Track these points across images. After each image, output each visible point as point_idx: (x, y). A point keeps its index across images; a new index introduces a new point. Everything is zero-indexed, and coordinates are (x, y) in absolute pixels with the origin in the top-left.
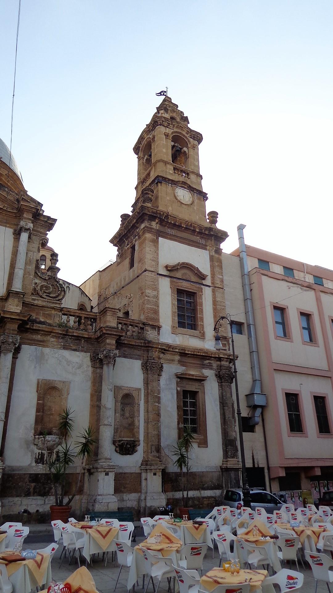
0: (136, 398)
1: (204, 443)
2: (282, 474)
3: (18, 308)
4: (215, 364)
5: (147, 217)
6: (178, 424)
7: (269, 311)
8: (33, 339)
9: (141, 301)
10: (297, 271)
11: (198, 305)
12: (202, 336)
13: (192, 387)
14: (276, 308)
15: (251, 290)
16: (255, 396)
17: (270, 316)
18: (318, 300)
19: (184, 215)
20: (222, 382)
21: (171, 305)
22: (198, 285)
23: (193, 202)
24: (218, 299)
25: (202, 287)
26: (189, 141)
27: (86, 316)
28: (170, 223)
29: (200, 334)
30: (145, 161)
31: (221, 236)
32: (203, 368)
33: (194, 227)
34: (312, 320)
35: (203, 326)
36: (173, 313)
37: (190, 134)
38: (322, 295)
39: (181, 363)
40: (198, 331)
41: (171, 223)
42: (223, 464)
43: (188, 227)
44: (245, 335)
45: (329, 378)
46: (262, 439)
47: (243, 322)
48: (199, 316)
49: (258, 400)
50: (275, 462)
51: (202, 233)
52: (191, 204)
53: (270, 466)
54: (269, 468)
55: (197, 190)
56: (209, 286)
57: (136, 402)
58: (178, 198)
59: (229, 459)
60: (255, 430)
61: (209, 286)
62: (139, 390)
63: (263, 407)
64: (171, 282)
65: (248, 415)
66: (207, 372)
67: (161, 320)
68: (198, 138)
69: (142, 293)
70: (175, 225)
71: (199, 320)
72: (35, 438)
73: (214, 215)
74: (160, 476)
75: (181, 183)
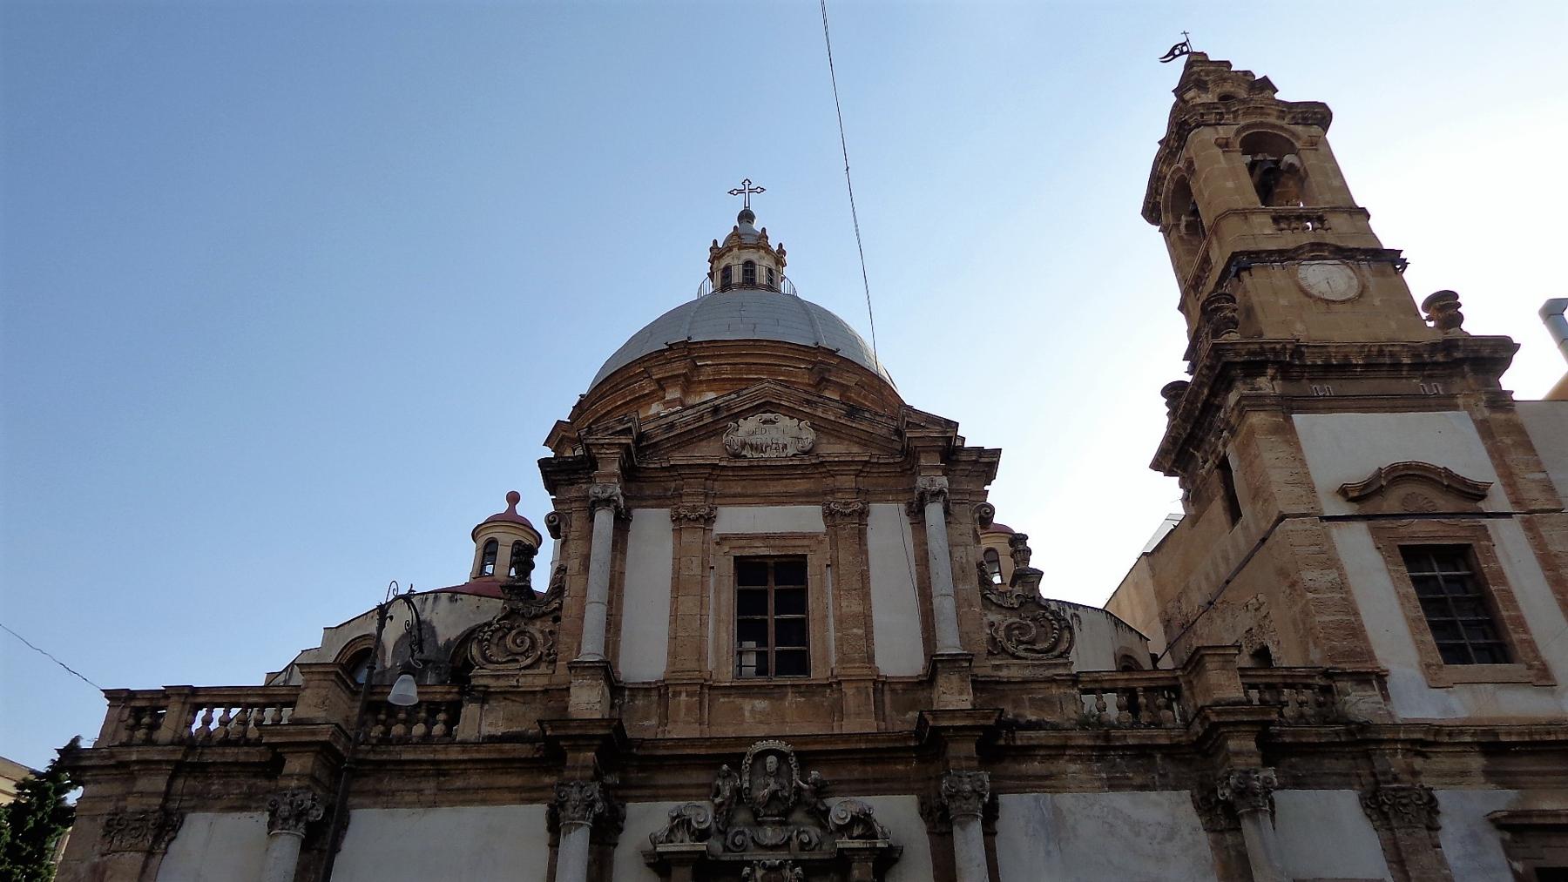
3: (965, 697)
9: (1296, 609)
27: (1145, 684)
36: (1412, 622)
41: (1314, 365)
48: (1505, 614)
52: (1361, 295)
55: (1366, 252)
56: (1508, 515)
61: (1508, 515)
64: (1374, 532)
67: (1378, 653)
69: (1293, 585)
71: (1510, 627)
73: (1446, 304)
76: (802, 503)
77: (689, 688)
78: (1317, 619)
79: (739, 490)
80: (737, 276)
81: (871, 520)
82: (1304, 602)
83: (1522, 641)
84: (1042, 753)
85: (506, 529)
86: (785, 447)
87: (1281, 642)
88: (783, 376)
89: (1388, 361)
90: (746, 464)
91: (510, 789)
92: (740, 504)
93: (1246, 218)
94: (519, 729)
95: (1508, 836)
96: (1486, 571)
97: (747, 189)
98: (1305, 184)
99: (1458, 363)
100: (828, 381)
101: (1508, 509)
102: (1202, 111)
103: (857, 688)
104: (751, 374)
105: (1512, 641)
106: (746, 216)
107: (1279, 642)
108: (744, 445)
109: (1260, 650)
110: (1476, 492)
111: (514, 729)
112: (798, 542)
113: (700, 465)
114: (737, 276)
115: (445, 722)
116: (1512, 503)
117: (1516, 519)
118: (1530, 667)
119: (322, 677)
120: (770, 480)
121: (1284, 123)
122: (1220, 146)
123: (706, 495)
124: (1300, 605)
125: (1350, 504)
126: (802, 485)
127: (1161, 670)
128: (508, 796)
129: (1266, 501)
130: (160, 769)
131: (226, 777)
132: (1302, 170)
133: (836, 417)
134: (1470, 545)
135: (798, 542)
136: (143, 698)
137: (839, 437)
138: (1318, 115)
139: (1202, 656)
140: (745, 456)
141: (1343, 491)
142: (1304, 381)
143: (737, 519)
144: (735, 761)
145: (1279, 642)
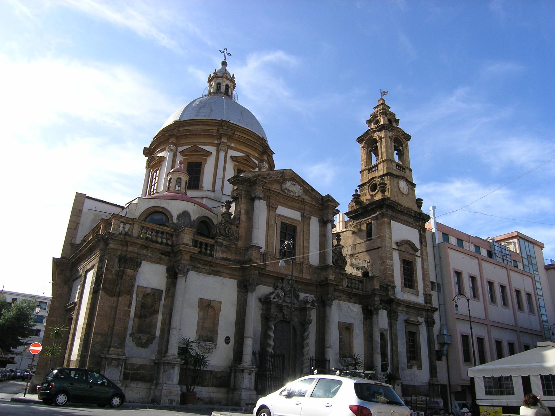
0: (386, 335)
1: (420, 367)
2: (460, 389)
3: (333, 276)
4: (424, 314)
5: (385, 206)
6: (407, 354)
7: (452, 273)
8: (111, 248)
9: (382, 268)
10: (465, 242)
11: (414, 271)
12: (417, 294)
13: (413, 329)
14: (456, 272)
15: (440, 258)
16: (445, 337)
17: (453, 278)
18: (480, 266)
19: (405, 203)
20: (429, 326)
21: (400, 272)
22: (413, 257)
23: (409, 192)
24: (425, 267)
25: (416, 257)
26: (403, 142)
27: (358, 279)
28: (400, 211)
29: (416, 292)
30: (368, 151)
31: (427, 218)
32: (418, 316)
33: (411, 212)
34: (506, 292)
35: (417, 286)
36: (401, 276)
37: (404, 136)
38: (482, 262)
39: (407, 313)
40: (415, 290)
41: (399, 210)
42: (430, 381)
43: (408, 213)
44: (436, 291)
45: (486, 325)
46: (446, 366)
47: (434, 281)
48: (415, 279)
49: (446, 339)
50: (454, 382)
51: (415, 217)
52: (408, 194)
53: (450, 384)
54: (450, 385)
55: (410, 181)
56: (419, 257)
57: (386, 338)
58: (401, 190)
59: (434, 378)
60: (442, 359)
61: (419, 257)
62: (386, 330)
63: (448, 344)
64: (399, 254)
65: (438, 349)
66: (421, 319)
67: (395, 282)
68: (408, 137)
69: (383, 262)
70: (400, 211)
71: (415, 282)
72: (340, 359)
73: (419, 202)
74: (400, 386)
75: (401, 177)
76: (297, 211)
77: (271, 257)
78: (388, 272)
79: (282, 201)
80: (223, 89)
81: (311, 220)
82: (385, 267)
83: (416, 285)
84: (339, 291)
85: (185, 176)
86: (295, 193)
87: (374, 273)
88: (256, 146)
89: (410, 214)
90: (287, 195)
91: (228, 274)
92: (283, 206)
93: (392, 163)
94: (229, 257)
95: (406, 324)
96: (414, 268)
97: (225, 52)
98: (402, 157)
99: (420, 218)
100: (266, 152)
101: (420, 256)
102: (389, 126)
103: (306, 266)
104: (248, 142)
105: (415, 285)
106: (224, 64)
107: (373, 272)
108: (286, 189)
109: (366, 272)
110: (416, 250)
111: (228, 257)
112: (296, 222)
113: (276, 192)
114: (223, 89)
115: (210, 250)
116: (421, 254)
117: (420, 258)
118: (416, 291)
119: (190, 232)
120: (290, 201)
121: (402, 137)
122: (390, 138)
123: (276, 201)
124: (384, 267)
125: (397, 246)
126: (297, 205)
127: (539, 347)
128: (227, 276)
129: (382, 240)
130: (137, 246)
131: (153, 252)
132: (402, 152)
133: (309, 189)
134: (413, 262)
135: (296, 222)
136: (124, 219)
137: (306, 194)
138: (408, 137)
139: (374, 277)
140: (286, 192)
141: (397, 243)
142: (395, 212)
143: (283, 211)
144: (282, 279)
145: (373, 272)
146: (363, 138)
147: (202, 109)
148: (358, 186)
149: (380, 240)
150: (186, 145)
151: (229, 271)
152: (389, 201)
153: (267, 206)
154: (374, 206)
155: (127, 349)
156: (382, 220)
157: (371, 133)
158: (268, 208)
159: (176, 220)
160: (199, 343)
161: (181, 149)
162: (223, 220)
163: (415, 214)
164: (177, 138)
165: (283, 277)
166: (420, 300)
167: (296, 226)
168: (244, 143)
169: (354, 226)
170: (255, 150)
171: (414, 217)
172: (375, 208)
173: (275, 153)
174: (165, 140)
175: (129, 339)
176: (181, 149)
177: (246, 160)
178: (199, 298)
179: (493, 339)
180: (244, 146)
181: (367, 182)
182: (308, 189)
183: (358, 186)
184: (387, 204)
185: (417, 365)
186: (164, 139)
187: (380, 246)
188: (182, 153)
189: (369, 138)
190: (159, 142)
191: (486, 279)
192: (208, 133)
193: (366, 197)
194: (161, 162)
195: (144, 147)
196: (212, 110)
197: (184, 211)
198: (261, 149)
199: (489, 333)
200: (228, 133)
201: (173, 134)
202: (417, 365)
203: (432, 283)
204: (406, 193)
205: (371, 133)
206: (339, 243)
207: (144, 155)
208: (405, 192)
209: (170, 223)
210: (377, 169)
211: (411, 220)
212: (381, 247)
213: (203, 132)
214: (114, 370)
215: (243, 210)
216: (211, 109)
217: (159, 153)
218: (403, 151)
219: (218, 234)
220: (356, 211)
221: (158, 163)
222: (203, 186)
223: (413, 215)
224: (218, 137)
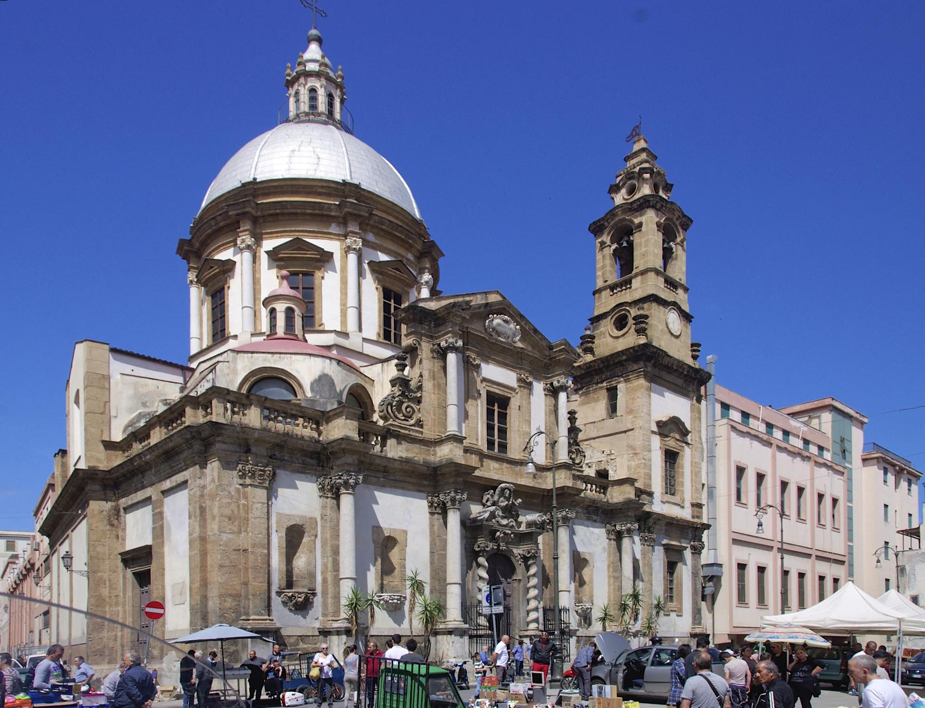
70: (666, 366)
82: (639, 462)
121: (678, 223)
124: (636, 463)
146: (603, 224)
147: (296, 153)
148: (590, 320)
149: (631, 416)
150: (282, 237)
151: (413, 480)
152: (652, 349)
153: (464, 362)
154: (624, 358)
155: (275, 614)
156: (637, 383)
157: (619, 213)
158: (466, 367)
159: (310, 392)
160: (381, 596)
161: (269, 244)
162: (396, 389)
163: (688, 372)
164: (255, 221)
165: (496, 485)
166: (686, 514)
167: (510, 398)
168: (390, 233)
169: (582, 393)
170: (409, 248)
171: (686, 376)
172: (625, 360)
173: (444, 253)
174: (228, 225)
175: (276, 601)
176: (269, 244)
177: (397, 269)
178: (373, 526)
179: (816, 574)
180: (391, 240)
181: (608, 312)
182: (527, 329)
183: (590, 320)
184: (649, 354)
185: (217, 459)
186: (227, 222)
187: (632, 428)
188: (273, 255)
189: (614, 224)
190: (214, 228)
191: (780, 477)
192: (320, 212)
193: (604, 339)
194: (226, 273)
195: (332, 253)
196: (319, 158)
197: (321, 374)
198: (421, 245)
199: (813, 567)
200: (360, 211)
201: (247, 213)
202: (217, 459)
203: (703, 485)
204: (678, 334)
205: (619, 213)
206: (573, 425)
207: (178, 256)
208: (676, 332)
209: (299, 397)
210: (630, 288)
211: (680, 382)
212: (633, 429)
213: (309, 210)
214: (263, 648)
215: (427, 372)
216: (317, 155)
217: (221, 251)
218: (676, 251)
219: (390, 415)
220: (588, 365)
221: (220, 275)
222: (324, 321)
223: (685, 373)
224: (341, 220)
